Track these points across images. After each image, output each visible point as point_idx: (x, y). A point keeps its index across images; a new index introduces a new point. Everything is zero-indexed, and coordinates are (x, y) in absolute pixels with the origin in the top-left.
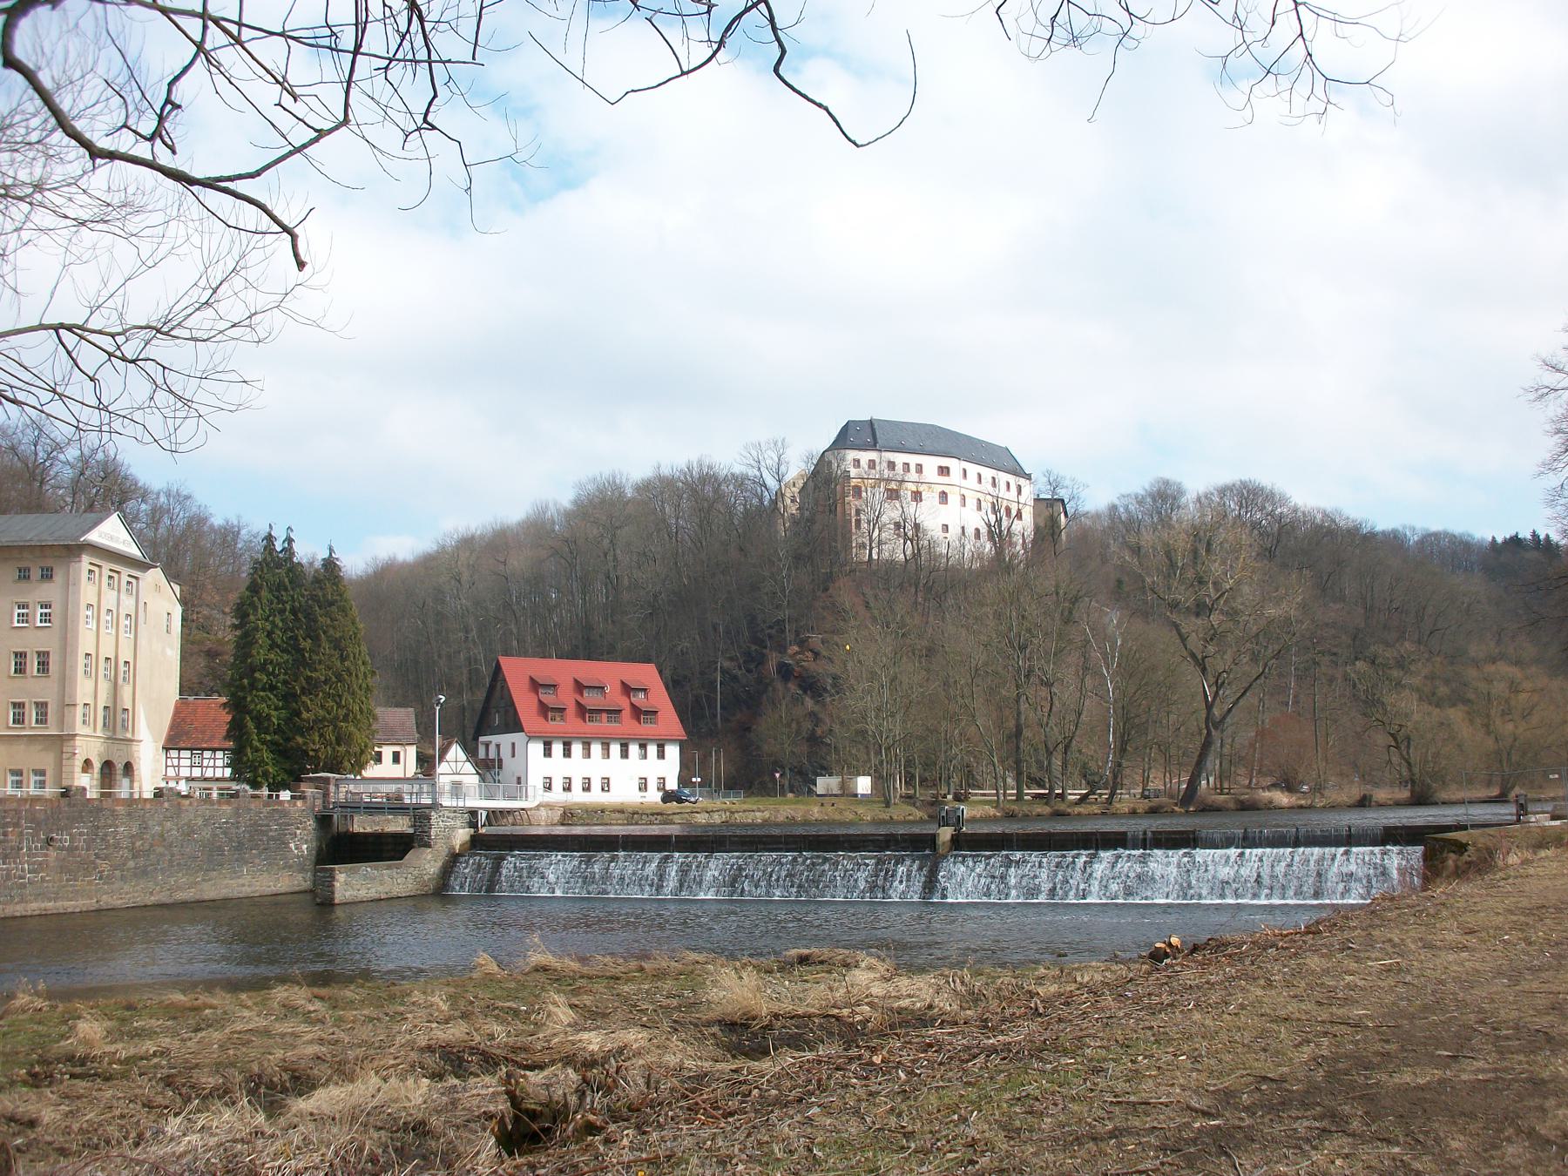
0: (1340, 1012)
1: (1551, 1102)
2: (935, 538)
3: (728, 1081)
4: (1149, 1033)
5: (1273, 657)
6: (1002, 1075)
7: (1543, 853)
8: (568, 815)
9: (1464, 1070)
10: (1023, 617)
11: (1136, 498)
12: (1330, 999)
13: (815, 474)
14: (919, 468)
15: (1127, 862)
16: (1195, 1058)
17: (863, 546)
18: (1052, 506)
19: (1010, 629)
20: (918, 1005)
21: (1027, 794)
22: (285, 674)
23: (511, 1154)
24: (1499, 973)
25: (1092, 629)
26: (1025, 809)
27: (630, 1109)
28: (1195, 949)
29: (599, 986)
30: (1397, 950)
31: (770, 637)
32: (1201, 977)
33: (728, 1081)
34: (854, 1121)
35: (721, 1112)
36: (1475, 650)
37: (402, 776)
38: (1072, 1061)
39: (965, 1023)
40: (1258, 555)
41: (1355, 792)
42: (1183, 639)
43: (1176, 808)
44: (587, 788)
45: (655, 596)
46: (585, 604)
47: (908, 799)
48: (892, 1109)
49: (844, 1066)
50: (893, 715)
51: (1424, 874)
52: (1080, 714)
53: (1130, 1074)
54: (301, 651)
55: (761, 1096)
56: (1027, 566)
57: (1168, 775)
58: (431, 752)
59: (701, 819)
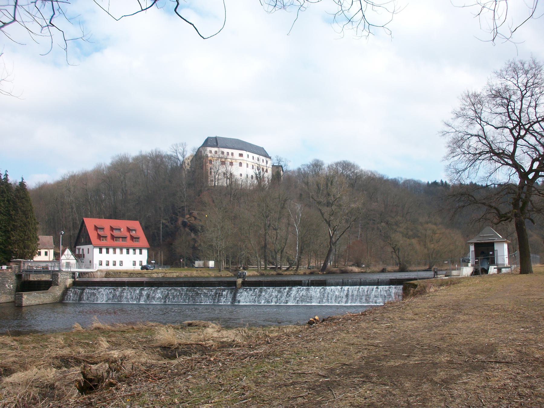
0: (371, 341)
1: (439, 370)
2: (237, 178)
3: (160, 367)
4: (306, 349)
5: (353, 221)
6: (255, 364)
7: (442, 288)
8: (108, 274)
9: (411, 360)
10: (267, 206)
11: (307, 166)
12: (368, 337)
13: (196, 155)
14: (232, 154)
15: (303, 291)
16: (321, 357)
17: (212, 181)
18: (278, 168)
19: (263, 210)
20: (230, 340)
21: (268, 267)
22: (5, 223)
23: (82, 394)
24: (425, 328)
25: (291, 211)
26: (267, 272)
27: (126, 377)
28: (324, 320)
29: (118, 334)
30: (392, 320)
31: (179, 212)
32: (325, 330)
33: (160, 367)
34: (203, 380)
35: (157, 378)
36: (421, 220)
37: (48, 260)
38: (279, 359)
39: (243, 346)
40: (348, 186)
41: (381, 267)
42: (322, 214)
43: (319, 272)
44: (114, 265)
45: (139, 197)
46: (114, 199)
47: (227, 269)
48: (217, 376)
49: (201, 361)
50: (222, 240)
51: (403, 295)
52: (287, 240)
53: (299, 363)
54: (10, 215)
55: (171, 372)
56: (269, 188)
57: (317, 261)
58: (59, 252)
59: (155, 275)
